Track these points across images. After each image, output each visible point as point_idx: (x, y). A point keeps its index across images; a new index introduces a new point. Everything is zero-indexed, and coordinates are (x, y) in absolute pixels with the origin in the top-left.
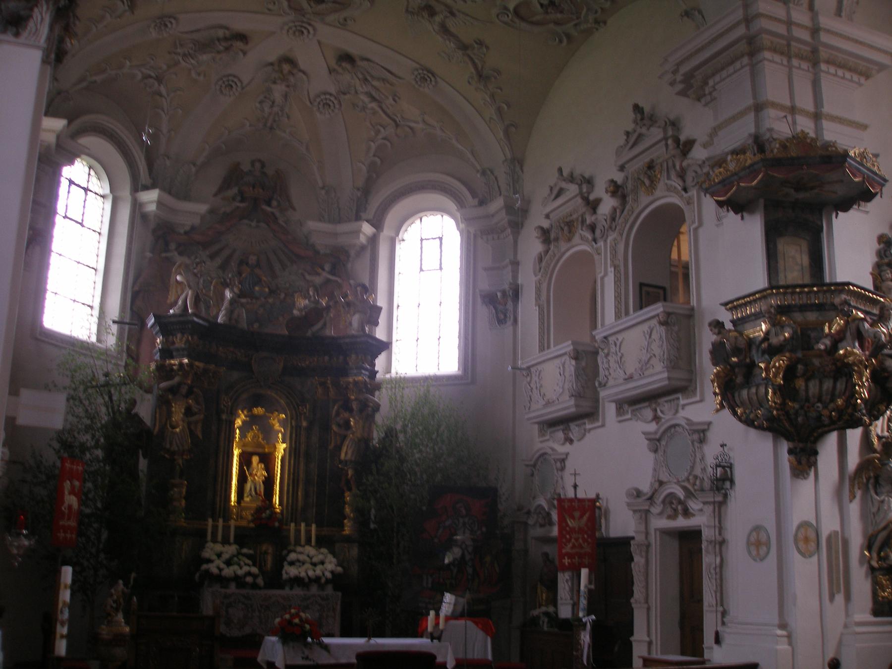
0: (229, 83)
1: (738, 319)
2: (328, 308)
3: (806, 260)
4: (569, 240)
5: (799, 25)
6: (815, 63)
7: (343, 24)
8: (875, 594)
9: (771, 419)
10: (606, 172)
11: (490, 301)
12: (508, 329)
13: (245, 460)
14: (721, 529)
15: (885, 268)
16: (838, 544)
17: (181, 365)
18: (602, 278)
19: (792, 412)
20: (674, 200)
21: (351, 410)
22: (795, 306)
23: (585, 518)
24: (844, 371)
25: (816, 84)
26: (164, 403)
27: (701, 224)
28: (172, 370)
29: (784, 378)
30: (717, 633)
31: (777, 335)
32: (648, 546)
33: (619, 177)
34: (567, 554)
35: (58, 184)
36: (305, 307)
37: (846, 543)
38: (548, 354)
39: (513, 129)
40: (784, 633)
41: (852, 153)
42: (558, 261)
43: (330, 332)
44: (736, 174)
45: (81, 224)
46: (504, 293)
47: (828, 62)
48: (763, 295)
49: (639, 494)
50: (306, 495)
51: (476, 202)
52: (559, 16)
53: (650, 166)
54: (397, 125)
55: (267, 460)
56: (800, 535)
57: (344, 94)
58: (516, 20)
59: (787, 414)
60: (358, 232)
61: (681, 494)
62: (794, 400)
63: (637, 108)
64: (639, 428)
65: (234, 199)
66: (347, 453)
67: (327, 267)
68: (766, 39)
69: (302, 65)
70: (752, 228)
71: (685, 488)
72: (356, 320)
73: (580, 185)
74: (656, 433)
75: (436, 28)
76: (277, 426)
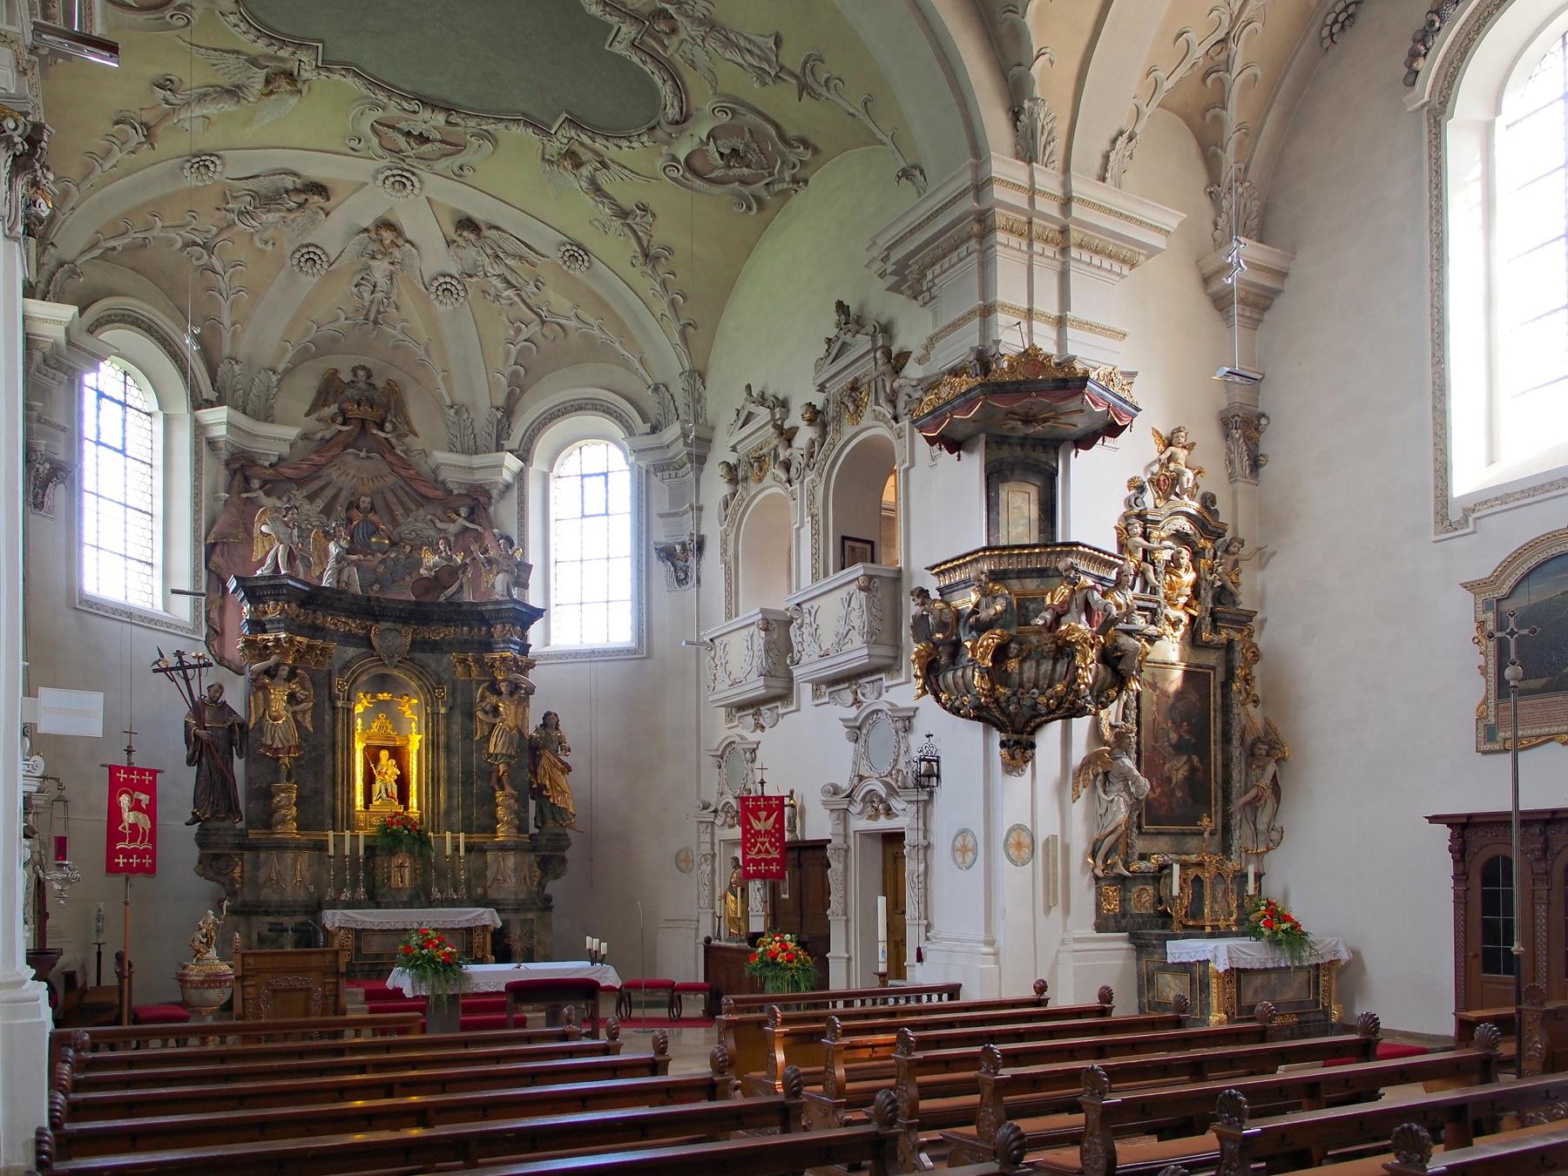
0: (310, 256)
1: (947, 587)
2: (465, 565)
3: (1034, 511)
4: (760, 480)
5: (1044, 194)
6: (1065, 250)
7: (459, 174)
8: (1098, 906)
9: (978, 707)
10: (803, 394)
11: (671, 557)
12: (690, 590)
13: (372, 755)
14: (926, 831)
15: (1134, 520)
16: (1056, 850)
17: (277, 640)
18: (798, 529)
19: (1002, 699)
20: (882, 431)
21: (500, 693)
22: (1012, 571)
23: (772, 819)
24: (1065, 650)
25: (1064, 276)
26: (258, 686)
27: (912, 464)
28: (266, 647)
29: (994, 659)
30: (919, 950)
31: (987, 607)
32: (847, 850)
33: (819, 400)
34: (752, 860)
35: (81, 395)
36: (435, 565)
37: (1066, 849)
38: (736, 622)
39: (690, 330)
40: (991, 950)
41: (1093, 375)
42: (747, 506)
43: (468, 597)
44: (948, 403)
45: (123, 452)
46: (683, 545)
47: (1080, 246)
48: (974, 557)
49: (836, 790)
50: (450, 796)
51: (647, 427)
52: (745, 170)
53: (854, 387)
54: (543, 322)
55: (398, 754)
56: (1011, 840)
57: (470, 276)
58: (688, 175)
59: (997, 701)
60: (499, 466)
61: (882, 791)
62: (1006, 685)
63: (841, 307)
64: (841, 710)
65: (333, 421)
66: (496, 745)
67: (463, 511)
68: (1001, 216)
69: (409, 236)
70: (972, 466)
71: (887, 785)
72: (500, 581)
73: (772, 409)
74: (856, 719)
75: (584, 185)
76: (408, 714)
